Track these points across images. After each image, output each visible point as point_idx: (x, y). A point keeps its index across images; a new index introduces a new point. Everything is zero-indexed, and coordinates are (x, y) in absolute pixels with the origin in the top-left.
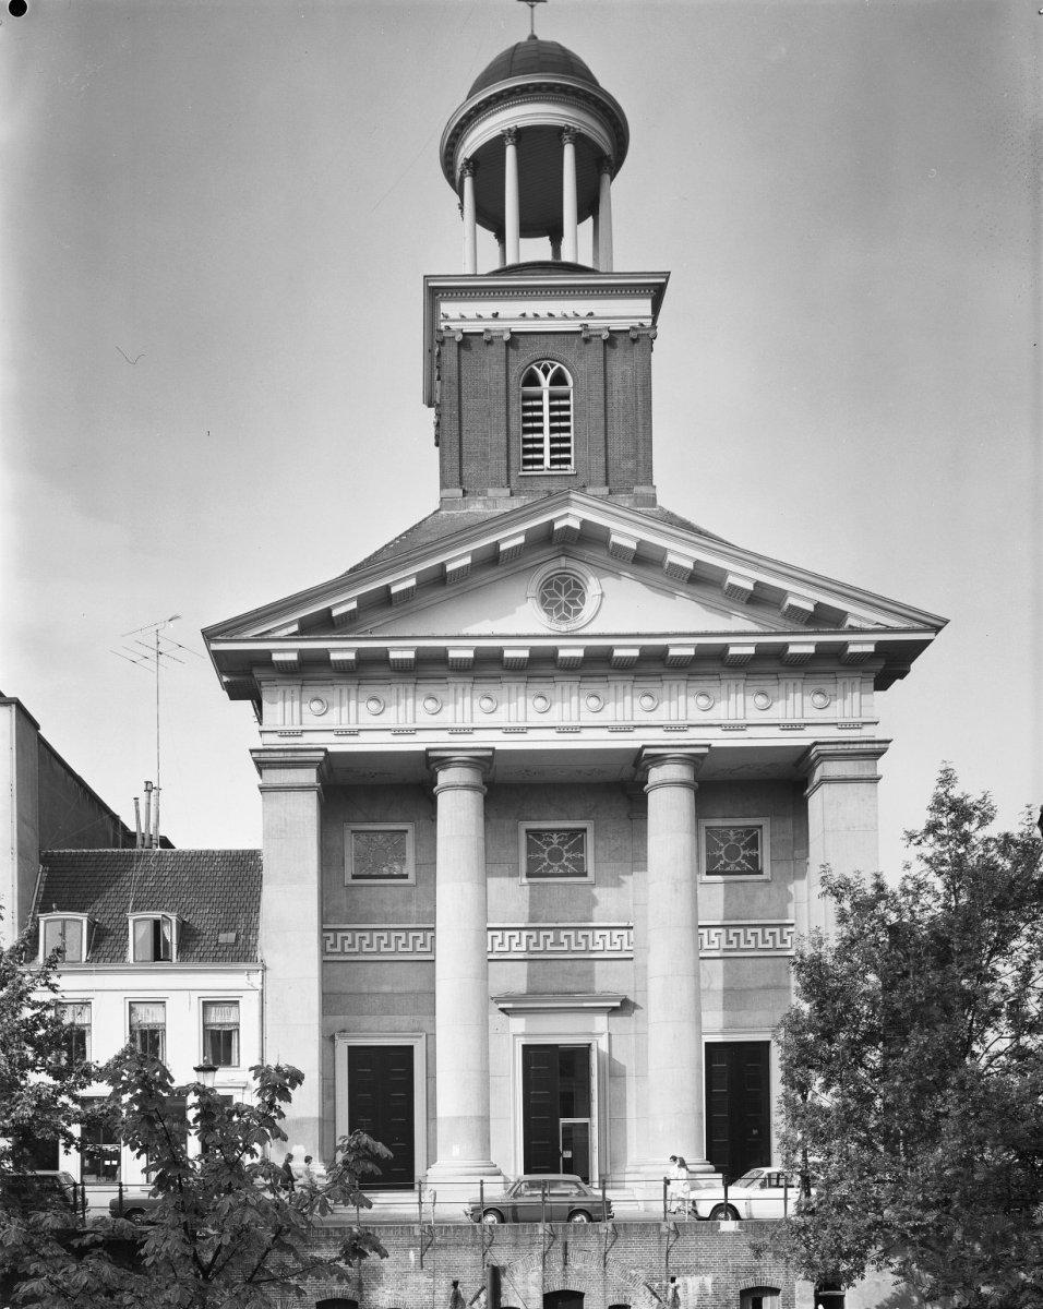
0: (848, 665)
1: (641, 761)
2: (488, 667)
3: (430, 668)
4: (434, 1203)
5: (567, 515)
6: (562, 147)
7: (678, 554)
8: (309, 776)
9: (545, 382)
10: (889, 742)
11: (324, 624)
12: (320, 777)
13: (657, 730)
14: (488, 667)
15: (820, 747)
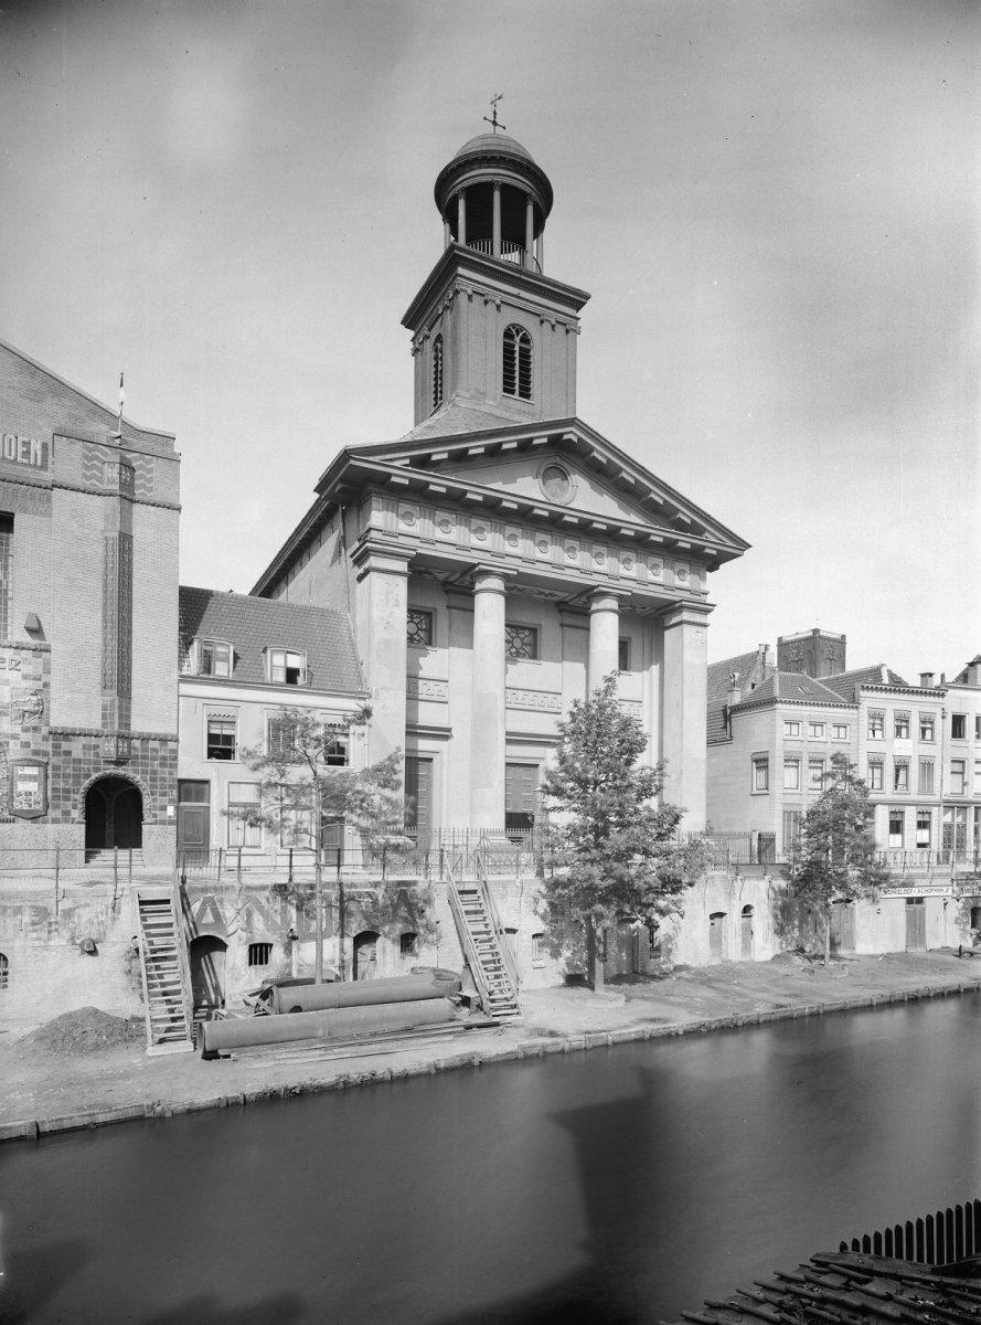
0: (560, 528)
1: (590, 594)
2: (524, 518)
3: (492, 511)
4: (115, 868)
5: (571, 432)
6: (526, 207)
7: (628, 473)
8: (402, 566)
9: (517, 339)
10: (714, 605)
11: (423, 463)
12: (409, 566)
13: (486, 554)
14: (524, 518)
15: (481, 566)
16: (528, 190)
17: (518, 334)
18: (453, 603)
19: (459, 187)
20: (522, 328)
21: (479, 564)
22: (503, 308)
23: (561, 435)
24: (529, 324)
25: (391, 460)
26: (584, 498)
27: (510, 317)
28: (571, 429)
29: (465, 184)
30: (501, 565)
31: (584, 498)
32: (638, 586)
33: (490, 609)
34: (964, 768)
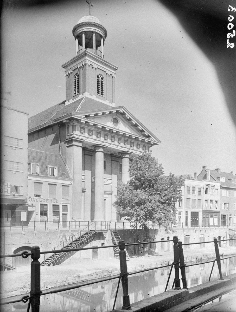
7: (140, 127)
9: (100, 78)
15: (74, 138)
16: (102, 35)
17: (100, 76)
18: (113, 159)
19: (83, 30)
20: (101, 75)
21: (99, 144)
22: (97, 69)
23: (119, 110)
24: (103, 74)
25: (81, 116)
26: (122, 127)
27: (99, 72)
28: (122, 109)
29: (85, 30)
30: (103, 145)
31: (122, 127)
32: (115, 146)
33: (100, 156)
34: (114, 255)
